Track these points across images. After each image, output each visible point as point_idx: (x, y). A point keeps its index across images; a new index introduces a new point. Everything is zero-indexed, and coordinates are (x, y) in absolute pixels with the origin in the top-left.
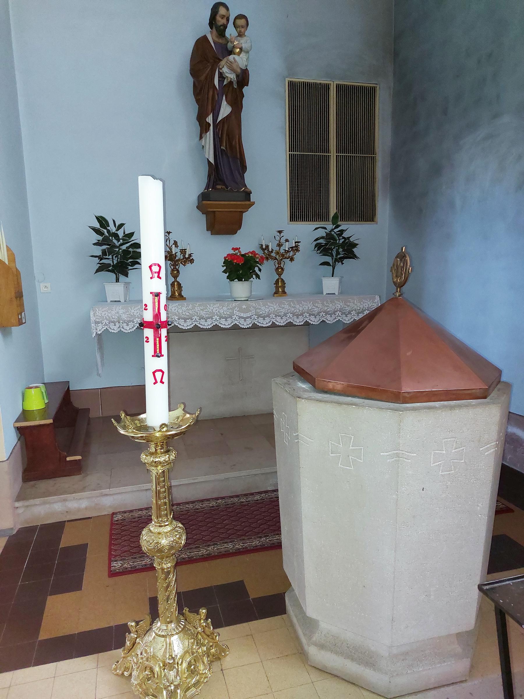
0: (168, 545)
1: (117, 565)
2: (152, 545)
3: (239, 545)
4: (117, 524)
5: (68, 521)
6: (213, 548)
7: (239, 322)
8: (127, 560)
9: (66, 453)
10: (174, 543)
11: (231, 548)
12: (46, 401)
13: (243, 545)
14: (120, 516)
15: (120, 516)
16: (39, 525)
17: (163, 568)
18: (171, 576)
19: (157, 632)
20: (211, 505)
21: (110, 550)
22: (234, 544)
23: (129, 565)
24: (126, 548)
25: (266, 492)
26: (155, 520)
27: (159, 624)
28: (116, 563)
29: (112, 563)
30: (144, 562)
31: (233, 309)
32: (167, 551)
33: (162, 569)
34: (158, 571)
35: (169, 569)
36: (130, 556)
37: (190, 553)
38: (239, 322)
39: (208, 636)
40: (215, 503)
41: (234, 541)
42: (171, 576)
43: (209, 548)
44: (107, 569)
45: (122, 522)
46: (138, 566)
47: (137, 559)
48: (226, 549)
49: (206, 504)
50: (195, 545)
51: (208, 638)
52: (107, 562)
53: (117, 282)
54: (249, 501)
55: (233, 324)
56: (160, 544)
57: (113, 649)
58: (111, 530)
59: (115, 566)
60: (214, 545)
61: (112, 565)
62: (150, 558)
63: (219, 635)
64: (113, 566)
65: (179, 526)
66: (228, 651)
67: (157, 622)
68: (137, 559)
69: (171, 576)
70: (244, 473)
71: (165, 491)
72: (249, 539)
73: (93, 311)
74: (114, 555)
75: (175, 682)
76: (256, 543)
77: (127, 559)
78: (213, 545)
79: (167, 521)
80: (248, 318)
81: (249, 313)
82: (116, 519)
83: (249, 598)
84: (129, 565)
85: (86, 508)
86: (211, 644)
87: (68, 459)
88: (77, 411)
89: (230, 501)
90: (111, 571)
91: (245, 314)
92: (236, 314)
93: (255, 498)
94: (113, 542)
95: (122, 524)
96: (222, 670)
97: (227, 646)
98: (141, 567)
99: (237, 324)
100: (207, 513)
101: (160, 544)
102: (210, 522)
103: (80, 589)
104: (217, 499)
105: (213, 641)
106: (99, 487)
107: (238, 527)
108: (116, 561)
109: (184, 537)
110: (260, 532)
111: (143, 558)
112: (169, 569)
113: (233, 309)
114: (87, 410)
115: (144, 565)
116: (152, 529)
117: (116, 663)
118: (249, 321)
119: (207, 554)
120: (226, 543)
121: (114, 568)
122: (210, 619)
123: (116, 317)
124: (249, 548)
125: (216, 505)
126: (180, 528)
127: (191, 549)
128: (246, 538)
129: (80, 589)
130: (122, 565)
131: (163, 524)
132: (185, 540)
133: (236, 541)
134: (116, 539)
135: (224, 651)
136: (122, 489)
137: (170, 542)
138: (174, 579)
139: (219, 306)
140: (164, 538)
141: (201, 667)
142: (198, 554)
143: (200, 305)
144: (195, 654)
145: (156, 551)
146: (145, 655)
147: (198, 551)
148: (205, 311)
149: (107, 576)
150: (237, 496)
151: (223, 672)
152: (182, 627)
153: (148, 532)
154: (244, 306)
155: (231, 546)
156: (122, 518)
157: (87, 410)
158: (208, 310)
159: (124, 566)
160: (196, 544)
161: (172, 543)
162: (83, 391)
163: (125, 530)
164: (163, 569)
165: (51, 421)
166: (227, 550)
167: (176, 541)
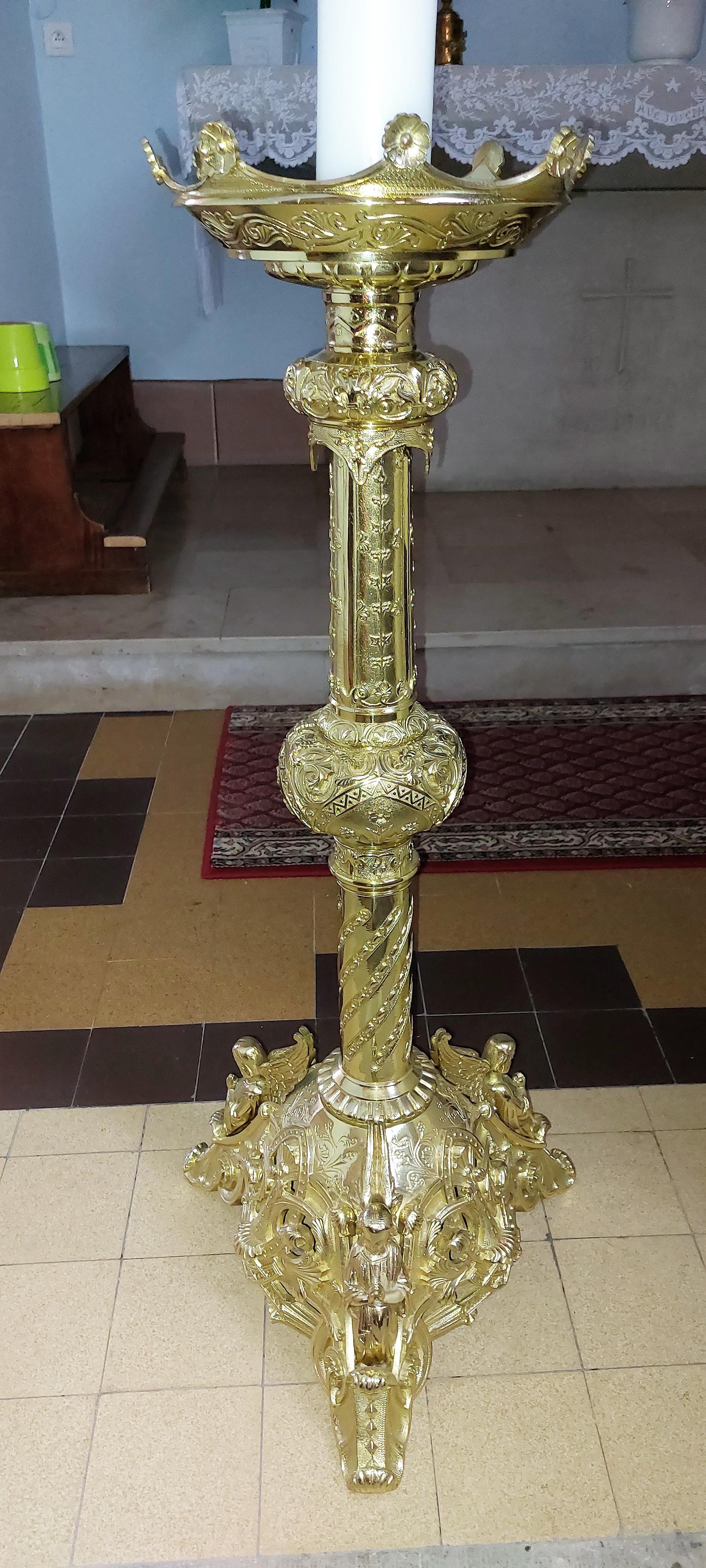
0: (390, 795)
1: (229, 847)
2: (324, 789)
3: (602, 840)
4: (239, 738)
5: (109, 714)
6: (517, 836)
7: (649, 143)
8: (259, 836)
9: (102, 527)
10: (414, 793)
11: (575, 845)
12: (53, 376)
13: (612, 839)
14: (250, 718)
15: (250, 718)
16: (30, 716)
17: (365, 885)
18: (397, 917)
19: (331, 1100)
20: (511, 717)
21: (214, 805)
22: (583, 834)
23: (263, 851)
24: (258, 805)
25: (683, 699)
26: (340, 690)
27: (338, 1074)
28: (227, 839)
29: (215, 839)
30: (308, 848)
31: (631, 93)
32: (384, 821)
33: (359, 889)
34: (344, 891)
35: (390, 892)
36: (268, 827)
37: (446, 841)
38: (649, 143)
39: (513, 1129)
40: (524, 713)
41: (584, 825)
42: (395, 916)
43: (505, 835)
44: (200, 853)
45: (255, 734)
46: (290, 858)
47: (290, 838)
48: (559, 844)
49: (495, 714)
50: (461, 820)
51: (510, 1134)
52: (202, 835)
53: (262, 7)
54: (628, 719)
55: (624, 154)
56: (357, 791)
57: (194, 1096)
58: (222, 749)
59: (223, 850)
60: (518, 828)
61: (214, 846)
62: (325, 841)
63: (548, 1124)
64: (217, 849)
65: (439, 731)
66: (570, 1176)
67: (334, 1065)
68: (290, 838)
69: (397, 917)
70: (624, 634)
71: (391, 560)
72: (632, 824)
73: (186, 84)
74: (223, 818)
75: (390, 1292)
76: (656, 838)
77: (259, 834)
78: (519, 830)
79: (392, 699)
80: (678, 129)
81: (685, 111)
82: (237, 723)
83: (641, 1006)
84: (263, 851)
85: (157, 686)
86: (520, 1154)
87: (110, 542)
88: (151, 437)
89: (569, 712)
90: (211, 862)
91: (671, 115)
92: (640, 113)
93: (649, 713)
94: (223, 783)
95: (254, 738)
96: (549, 1237)
97: (568, 1158)
98: (297, 861)
99: (642, 150)
100: (498, 739)
101: (357, 791)
102: (508, 764)
103: (117, 899)
104: (532, 703)
105: (525, 1143)
106: (190, 629)
107: (596, 788)
108: (228, 835)
109: (458, 778)
110: (668, 811)
111: (305, 837)
112: (390, 892)
113: (631, 93)
114: (180, 438)
115: (307, 856)
116: (325, 725)
117: (195, 1151)
118: (681, 141)
119: (499, 853)
120: (558, 827)
121: (221, 854)
122: (520, 1075)
123: (254, 109)
124: (633, 851)
125: (526, 718)
126: (443, 737)
127: (449, 831)
128: (623, 821)
129: (117, 899)
130: (244, 849)
131: (372, 712)
132: (460, 788)
133: (589, 825)
134: (234, 777)
135: (560, 1175)
136: (254, 642)
137: (401, 788)
138: (404, 928)
139: (585, 81)
140: (377, 770)
141: (483, 1241)
142: (470, 847)
143: (522, 76)
144: (467, 1198)
145: (338, 813)
146: (286, 1169)
147: (471, 841)
148: (536, 97)
149: (199, 876)
150: (592, 702)
151: (552, 1247)
152: (425, 1096)
153: (312, 736)
154: (673, 82)
155: (575, 838)
156: (255, 722)
157: (180, 438)
158: (549, 93)
159: (250, 853)
160: (466, 818)
161: (408, 790)
162: (168, 384)
163: (261, 757)
164: (362, 887)
165: (54, 418)
166: (562, 848)
167: (424, 786)
